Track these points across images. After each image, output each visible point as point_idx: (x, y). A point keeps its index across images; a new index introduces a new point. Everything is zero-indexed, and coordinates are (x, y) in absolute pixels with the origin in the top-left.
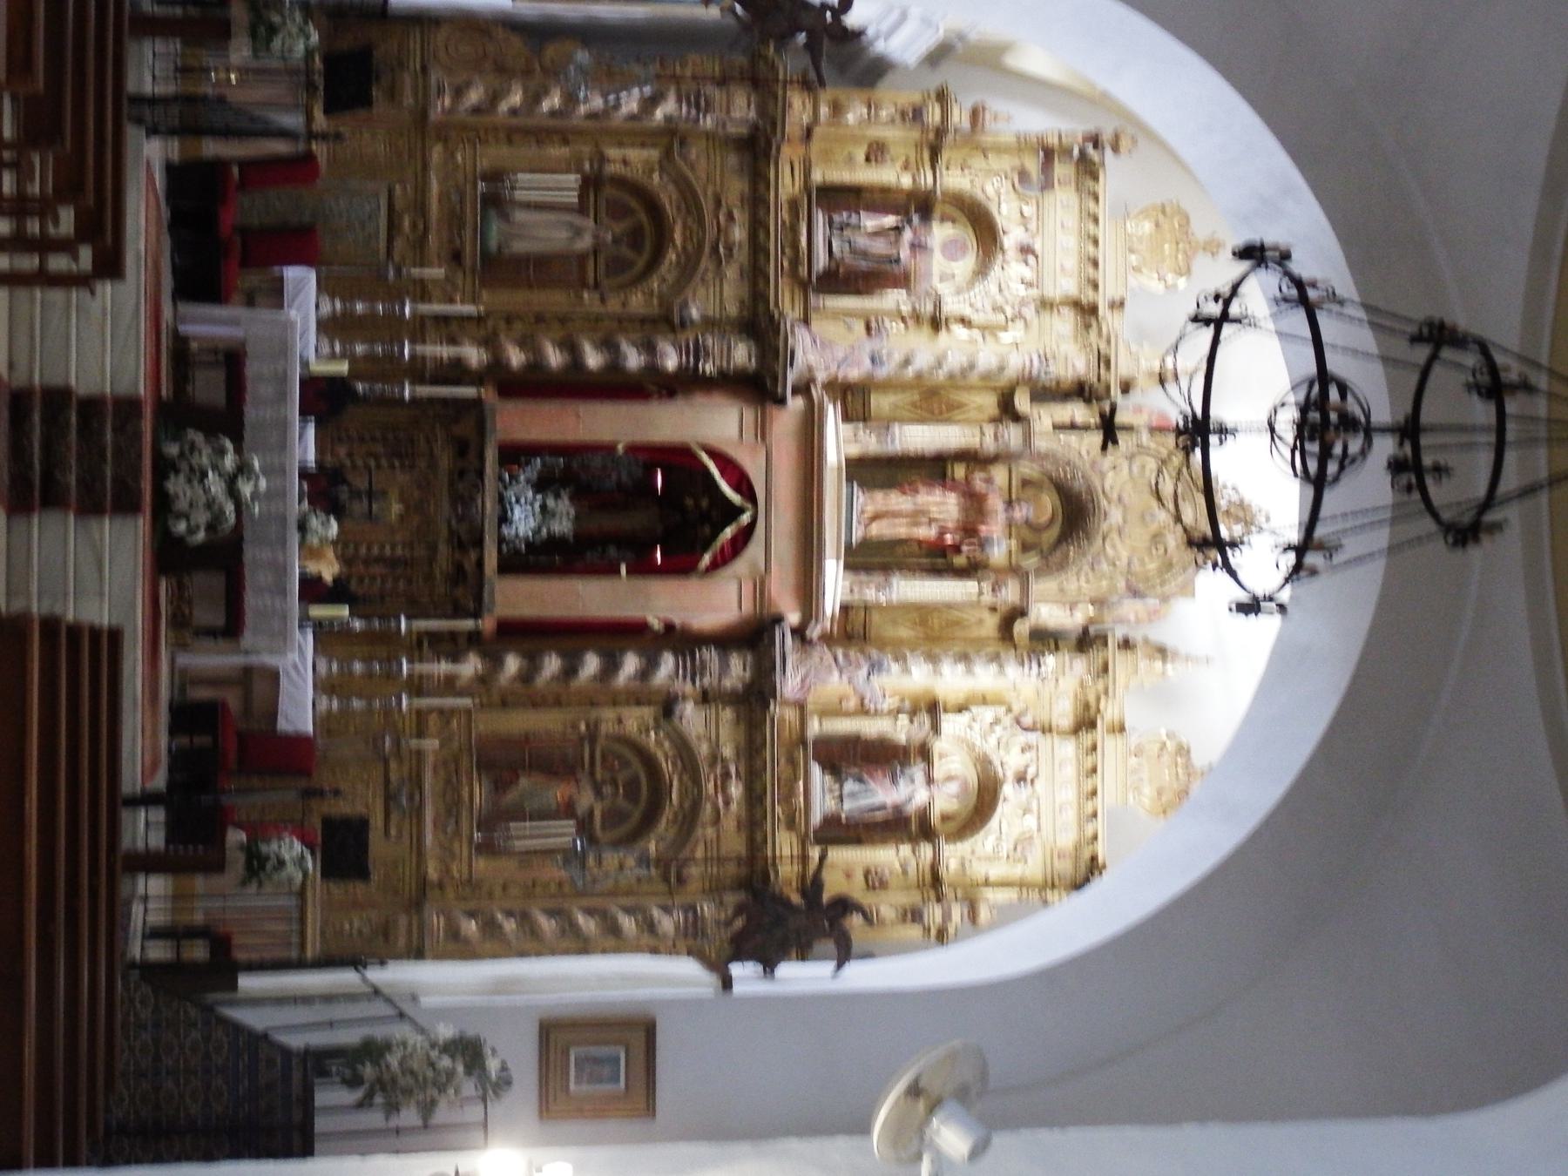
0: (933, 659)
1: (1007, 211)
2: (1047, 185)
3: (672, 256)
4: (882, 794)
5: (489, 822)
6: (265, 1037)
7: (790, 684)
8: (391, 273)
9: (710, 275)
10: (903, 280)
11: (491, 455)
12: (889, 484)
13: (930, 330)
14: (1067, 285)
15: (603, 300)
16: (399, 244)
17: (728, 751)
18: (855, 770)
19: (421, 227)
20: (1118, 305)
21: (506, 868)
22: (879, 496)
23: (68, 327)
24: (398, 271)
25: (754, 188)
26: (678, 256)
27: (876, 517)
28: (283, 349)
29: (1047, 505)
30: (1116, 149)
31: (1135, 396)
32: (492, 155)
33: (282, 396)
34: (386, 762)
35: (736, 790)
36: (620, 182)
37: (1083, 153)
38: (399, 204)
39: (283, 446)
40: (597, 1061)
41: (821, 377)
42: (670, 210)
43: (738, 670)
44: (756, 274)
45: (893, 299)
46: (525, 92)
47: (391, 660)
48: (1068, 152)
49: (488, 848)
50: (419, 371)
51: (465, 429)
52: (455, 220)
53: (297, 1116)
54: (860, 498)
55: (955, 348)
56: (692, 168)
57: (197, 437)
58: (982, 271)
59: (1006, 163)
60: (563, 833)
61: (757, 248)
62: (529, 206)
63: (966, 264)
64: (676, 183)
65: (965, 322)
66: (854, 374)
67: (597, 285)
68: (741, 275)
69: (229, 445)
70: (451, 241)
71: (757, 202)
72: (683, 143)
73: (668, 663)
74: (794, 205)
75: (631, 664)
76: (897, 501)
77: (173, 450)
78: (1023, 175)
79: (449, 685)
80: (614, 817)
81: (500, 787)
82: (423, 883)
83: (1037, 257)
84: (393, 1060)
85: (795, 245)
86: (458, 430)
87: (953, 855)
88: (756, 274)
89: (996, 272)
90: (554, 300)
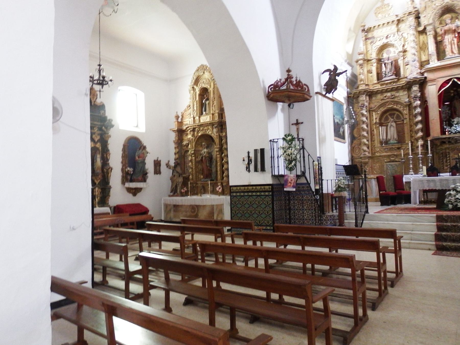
1: (379, 44)
2: (373, 37)
3: (395, 107)
8: (403, 160)
9: (399, 98)
10: (396, 61)
11: (444, 136)
12: (444, 52)
13: (407, 52)
14: (394, 28)
15: (406, 119)
16: (397, 160)
19: (393, 156)
20: (397, 16)
22: (447, 53)
23: (416, 234)
24: (402, 159)
25: (379, 93)
26: (395, 105)
27: (452, 52)
28: (421, 181)
29: (447, 17)
30: (364, 26)
31: (417, 6)
32: (377, 144)
33: (433, 181)
36: (380, 119)
37: (366, 32)
38: (389, 160)
39: (447, 180)
41: (419, 71)
42: (385, 108)
44: (397, 89)
45: (401, 62)
46: (363, 139)
48: (366, 36)
50: (425, 153)
51: (438, 143)
52: (391, 149)
54: (448, 56)
55: (411, 48)
56: (376, 106)
57: (446, 200)
58: (392, 45)
59: (369, 47)
61: (392, 90)
62: (387, 136)
63: (391, 49)
64: (379, 109)
65: (403, 46)
66: (418, 65)
67: (403, 121)
68: (398, 92)
69: (448, 193)
70: (396, 150)
71: (382, 92)
72: (371, 108)
74: (382, 85)
76: (448, 50)
77: (450, 206)
78: (371, 43)
83: (388, 35)
85: (390, 83)
86: (439, 144)
88: (397, 89)
89: (393, 42)
90: (407, 129)
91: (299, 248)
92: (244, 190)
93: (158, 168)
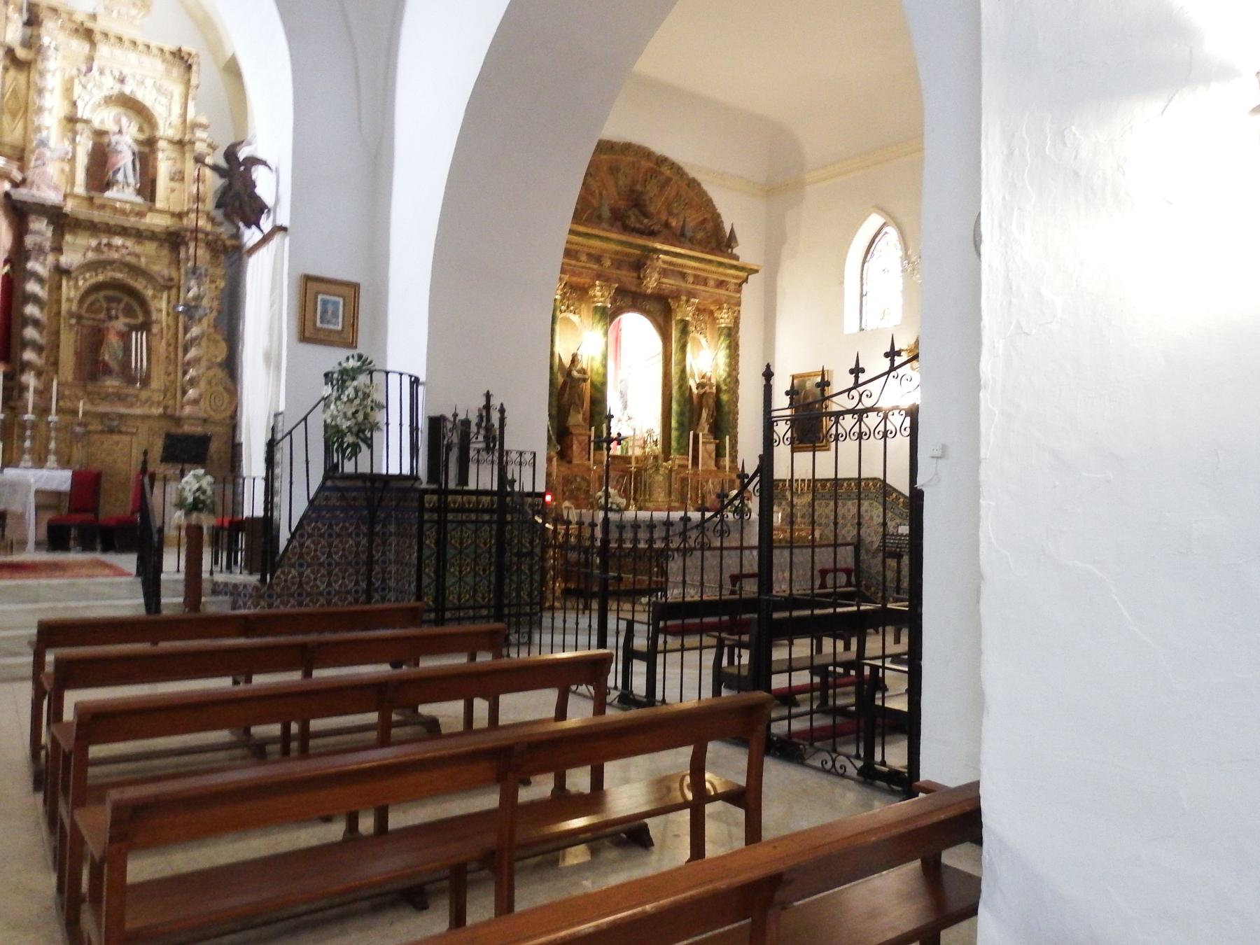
0: (40, 110)
4: (125, 160)
5: (130, 380)
6: (311, 502)
7: (51, 196)
17: (94, 243)
18: (111, 173)
21: (154, 374)
34: (89, 432)
35: (118, 241)
40: (324, 312)
42: (101, 278)
43: (40, 228)
47: (23, 426)
49: (146, 381)
53: (359, 484)
60: (138, 340)
73: (32, 265)
75: (32, 287)
79: (43, 393)
80: (129, 312)
81: (107, 371)
82: (164, 416)
84: (345, 425)
87: (167, 128)
91: (295, 676)
92: (467, 506)
93: (604, 426)
